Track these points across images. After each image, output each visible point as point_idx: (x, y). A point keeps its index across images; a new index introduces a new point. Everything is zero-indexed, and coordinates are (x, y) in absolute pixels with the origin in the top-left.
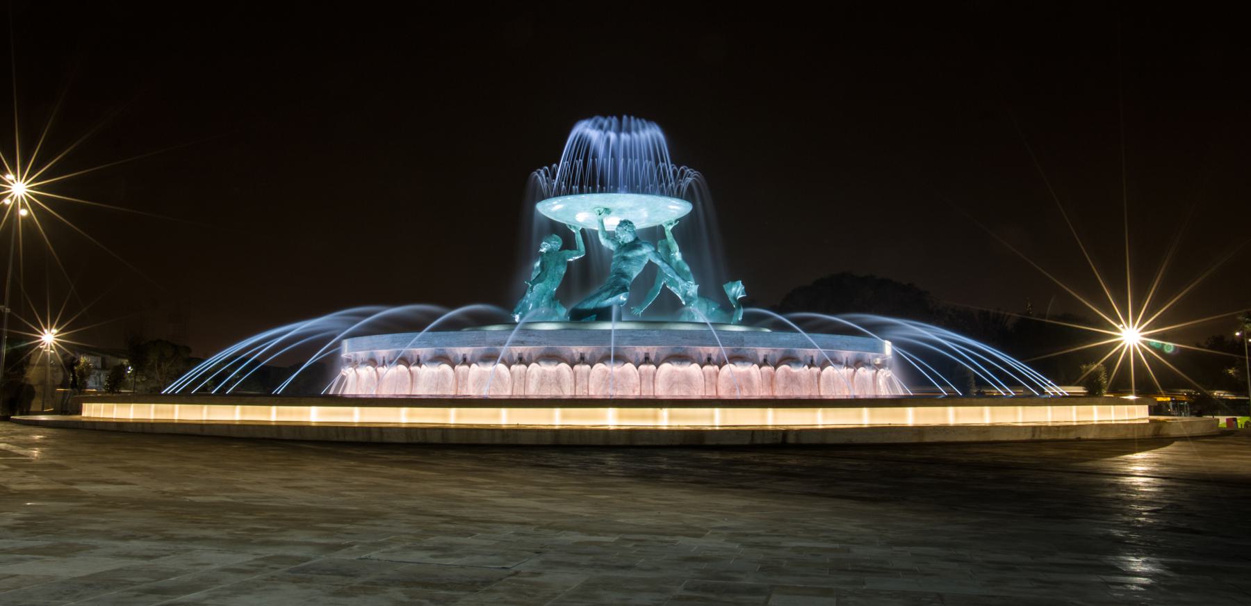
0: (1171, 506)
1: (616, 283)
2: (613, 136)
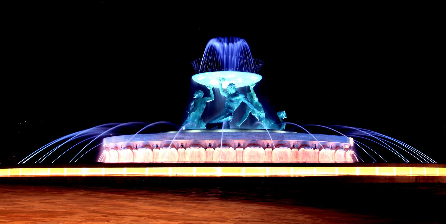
1: (227, 112)
2: (226, 45)
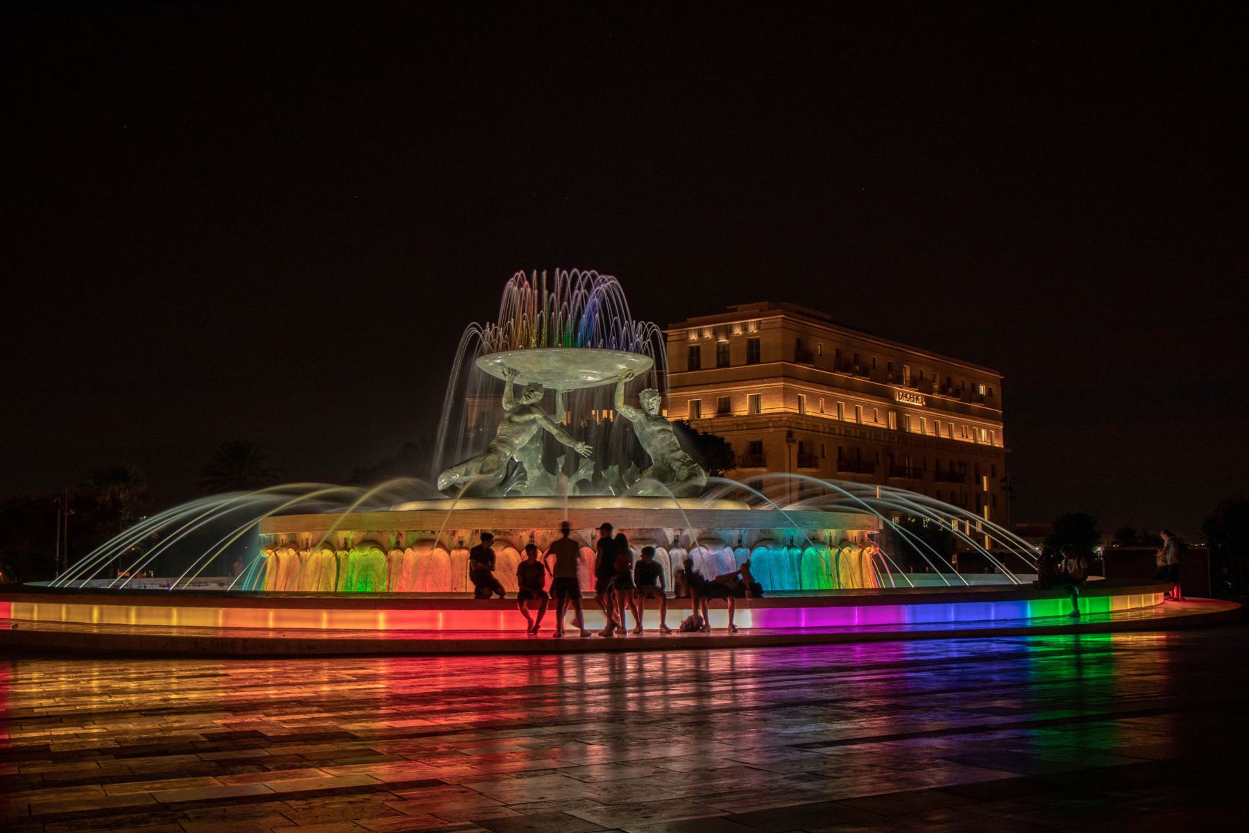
0: (695, 770)
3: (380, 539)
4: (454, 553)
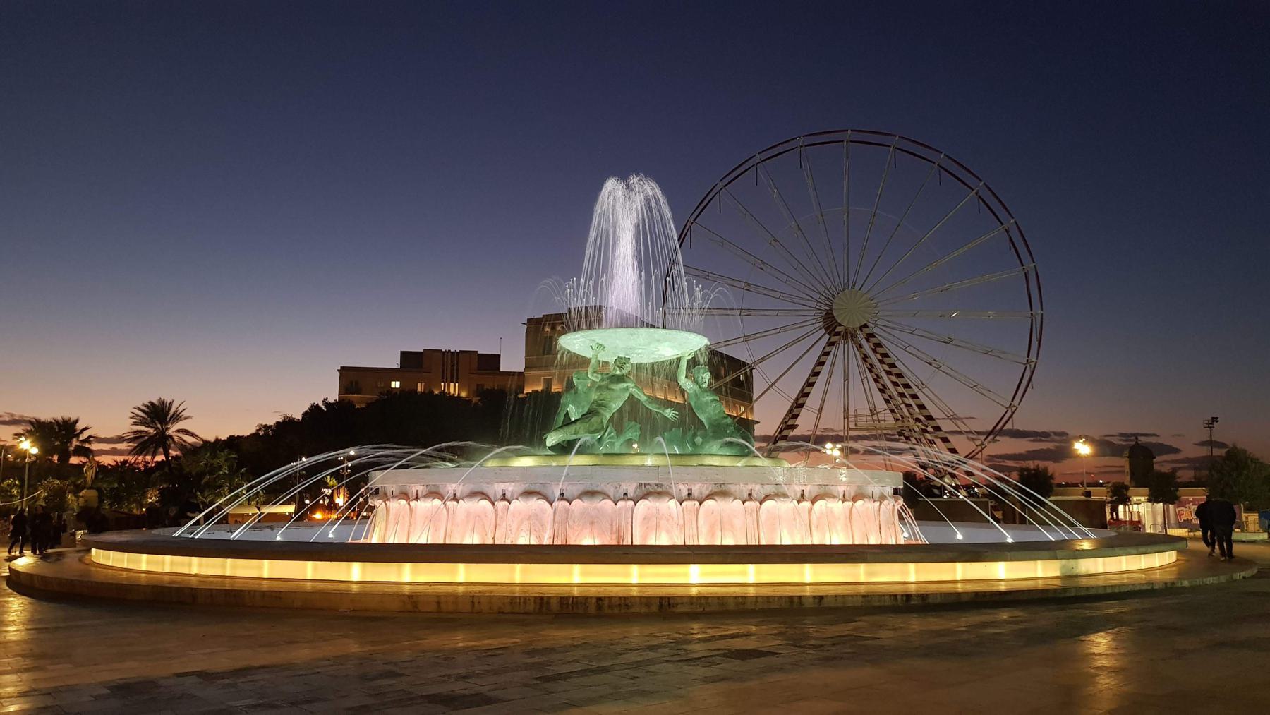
3: (543, 491)
4: (556, 504)
